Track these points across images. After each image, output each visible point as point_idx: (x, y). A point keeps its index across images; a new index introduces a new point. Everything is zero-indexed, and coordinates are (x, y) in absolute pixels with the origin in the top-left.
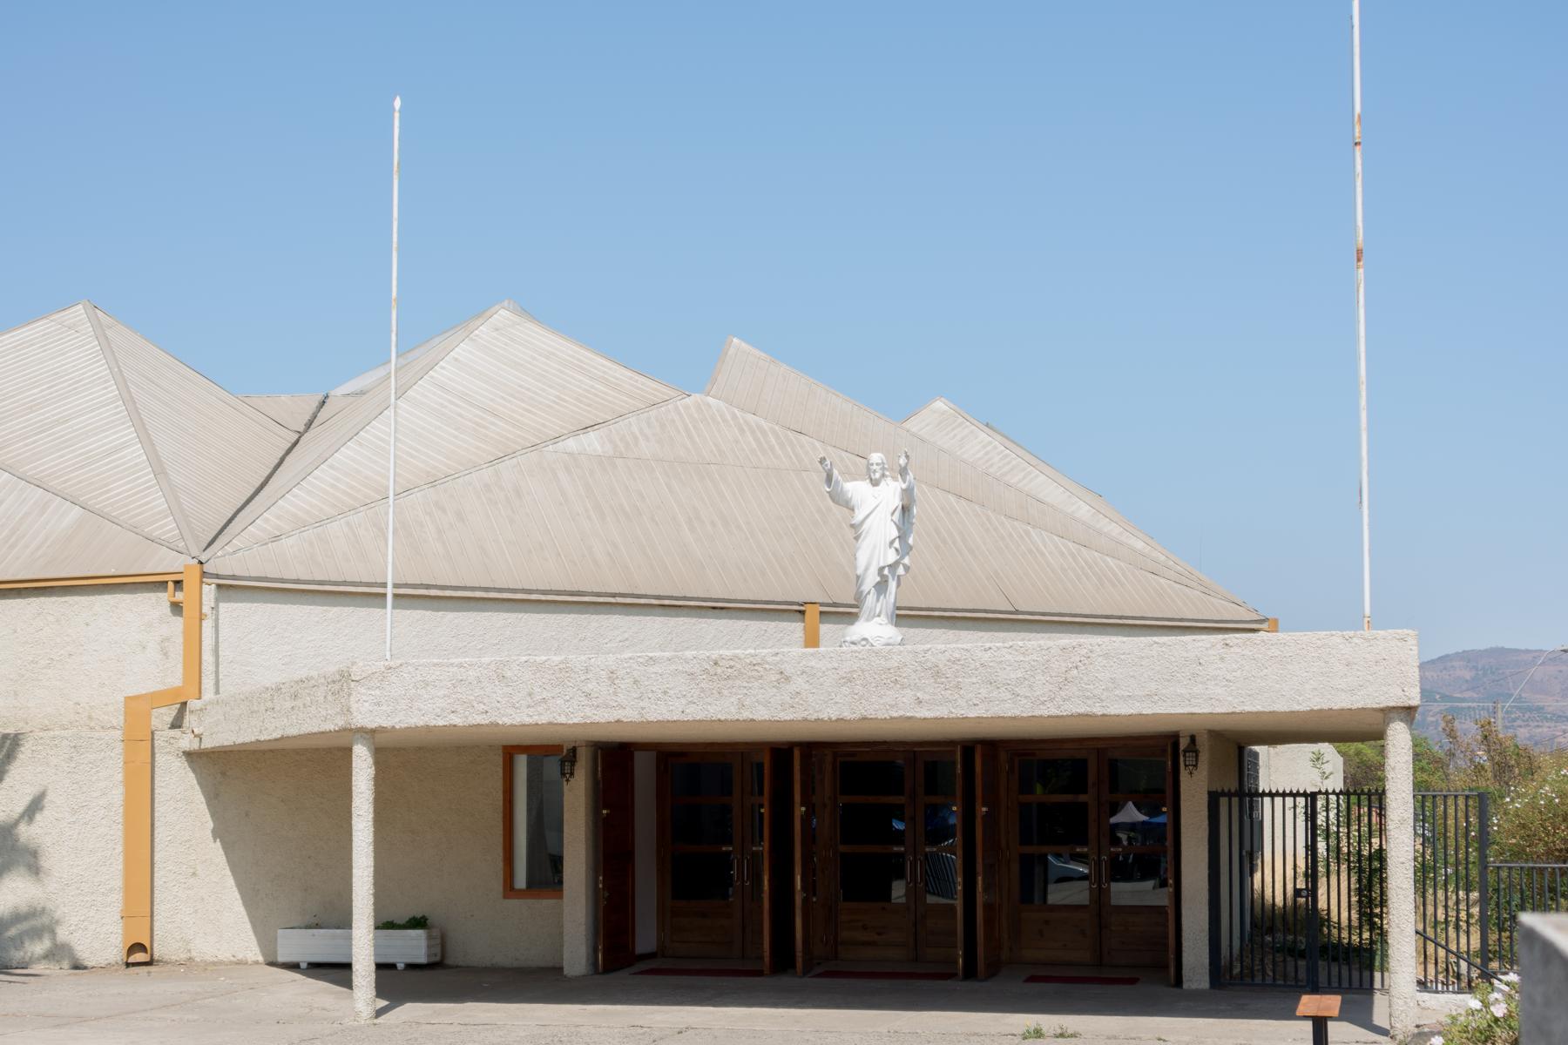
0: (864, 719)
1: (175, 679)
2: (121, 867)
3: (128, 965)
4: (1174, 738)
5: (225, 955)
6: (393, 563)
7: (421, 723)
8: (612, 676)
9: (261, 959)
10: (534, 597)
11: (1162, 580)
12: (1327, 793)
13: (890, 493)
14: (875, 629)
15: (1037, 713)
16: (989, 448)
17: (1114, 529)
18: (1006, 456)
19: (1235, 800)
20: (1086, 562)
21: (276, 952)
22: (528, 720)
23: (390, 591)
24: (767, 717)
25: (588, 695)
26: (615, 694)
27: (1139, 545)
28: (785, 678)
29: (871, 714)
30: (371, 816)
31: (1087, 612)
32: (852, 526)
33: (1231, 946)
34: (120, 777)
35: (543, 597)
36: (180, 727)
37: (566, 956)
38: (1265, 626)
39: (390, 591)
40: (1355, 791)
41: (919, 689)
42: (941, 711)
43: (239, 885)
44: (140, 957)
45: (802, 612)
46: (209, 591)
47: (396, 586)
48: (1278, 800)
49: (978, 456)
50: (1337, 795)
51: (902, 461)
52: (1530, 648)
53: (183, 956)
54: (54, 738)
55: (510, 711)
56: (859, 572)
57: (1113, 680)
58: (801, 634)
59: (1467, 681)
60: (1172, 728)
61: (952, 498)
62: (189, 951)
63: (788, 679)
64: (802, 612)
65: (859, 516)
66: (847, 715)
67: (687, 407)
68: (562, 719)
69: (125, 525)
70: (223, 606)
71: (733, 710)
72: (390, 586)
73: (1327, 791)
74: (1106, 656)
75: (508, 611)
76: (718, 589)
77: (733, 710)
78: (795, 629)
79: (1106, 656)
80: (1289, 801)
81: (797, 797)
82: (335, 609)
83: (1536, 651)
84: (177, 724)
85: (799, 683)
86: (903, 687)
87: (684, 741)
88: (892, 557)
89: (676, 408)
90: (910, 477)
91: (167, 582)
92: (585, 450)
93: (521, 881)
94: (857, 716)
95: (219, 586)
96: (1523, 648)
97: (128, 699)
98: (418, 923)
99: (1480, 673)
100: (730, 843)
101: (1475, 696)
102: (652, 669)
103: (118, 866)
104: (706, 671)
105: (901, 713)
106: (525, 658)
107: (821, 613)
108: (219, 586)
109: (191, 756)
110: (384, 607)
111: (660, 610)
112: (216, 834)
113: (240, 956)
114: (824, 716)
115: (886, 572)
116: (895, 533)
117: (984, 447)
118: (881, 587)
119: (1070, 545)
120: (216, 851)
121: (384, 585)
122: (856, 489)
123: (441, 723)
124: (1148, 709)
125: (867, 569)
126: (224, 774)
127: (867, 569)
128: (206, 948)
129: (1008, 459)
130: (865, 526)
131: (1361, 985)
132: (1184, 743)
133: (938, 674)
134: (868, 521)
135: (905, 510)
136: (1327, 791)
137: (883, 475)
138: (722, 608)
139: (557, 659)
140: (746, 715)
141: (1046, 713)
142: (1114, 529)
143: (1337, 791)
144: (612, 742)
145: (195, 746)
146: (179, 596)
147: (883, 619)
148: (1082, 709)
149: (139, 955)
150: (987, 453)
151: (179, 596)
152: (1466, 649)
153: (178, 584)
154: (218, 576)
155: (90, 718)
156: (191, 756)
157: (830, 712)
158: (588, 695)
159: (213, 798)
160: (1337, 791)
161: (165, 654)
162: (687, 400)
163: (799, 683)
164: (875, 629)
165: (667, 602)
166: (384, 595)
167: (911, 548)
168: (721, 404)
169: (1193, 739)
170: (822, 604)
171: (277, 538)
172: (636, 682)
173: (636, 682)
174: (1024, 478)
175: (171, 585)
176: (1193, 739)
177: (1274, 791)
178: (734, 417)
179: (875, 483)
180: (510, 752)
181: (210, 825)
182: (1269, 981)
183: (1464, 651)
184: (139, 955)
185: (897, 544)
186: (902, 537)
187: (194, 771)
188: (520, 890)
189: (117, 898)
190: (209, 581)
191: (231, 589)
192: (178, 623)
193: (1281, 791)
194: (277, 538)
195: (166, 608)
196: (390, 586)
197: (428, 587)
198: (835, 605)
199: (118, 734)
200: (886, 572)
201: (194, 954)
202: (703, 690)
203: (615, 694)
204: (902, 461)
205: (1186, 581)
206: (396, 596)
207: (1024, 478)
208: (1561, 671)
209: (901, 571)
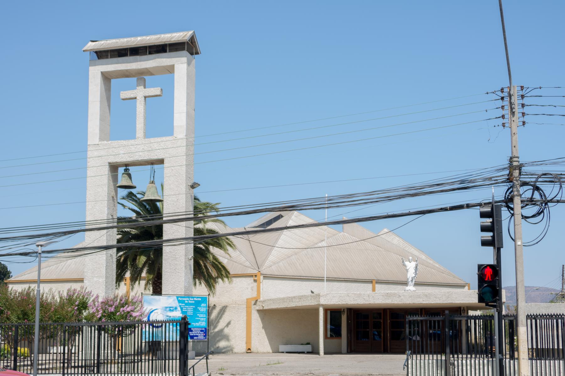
0: (414, 303)
1: (255, 295)
2: (246, 333)
3: (247, 353)
4: (460, 308)
5: (265, 351)
6: (326, 274)
7: (333, 304)
8: (369, 296)
9: (271, 351)
10: (320, 278)
11: (444, 275)
13: (413, 264)
14: (411, 288)
15: (443, 302)
16: (399, 241)
17: (431, 262)
18: (404, 243)
20: (428, 270)
21: (279, 349)
23: (325, 279)
24: (397, 303)
25: (364, 299)
26: (369, 299)
27: (437, 266)
28: (400, 296)
29: (415, 303)
30: (323, 320)
31: (430, 282)
32: (407, 270)
34: (245, 315)
35: (335, 279)
36: (256, 305)
37: (342, 349)
38: (467, 285)
39: (325, 279)
41: (423, 298)
42: (427, 302)
43: (268, 338)
44: (249, 351)
45: (372, 282)
46: (262, 277)
47: (326, 278)
49: (397, 243)
51: (417, 259)
52: (530, 286)
53: (257, 351)
54: (234, 307)
55: (350, 302)
56: (408, 278)
57: (456, 297)
58: (372, 286)
59: (509, 297)
61: (398, 256)
62: (258, 350)
63: (400, 297)
64: (372, 282)
65: (408, 268)
66: (411, 303)
67: (341, 235)
68: (360, 303)
70: (264, 281)
71: (391, 302)
72: (325, 280)
74: (455, 293)
75: (345, 282)
76: (355, 277)
77: (391, 302)
78: (370, 286)
79: (455, 293)
81: (388, 319)
82: (284, 281)
83: (532, 287)
84: (255, 304)
85: (402, 297)
86: (421, 298)
87: (362, 308)
88: (414, 275)
89: (339, 236)
90: (418, 262)
91: (253, 276)
92: (315, 243)
93: (329, 336)
94: (412, 303)
95: (264, 276)
96: (527, 286)
98: (308, 344)
99: (513, 294)
100: (369, 329)
101: (512, 302)
102: (376, 295)
103: (245, 333)
104: (386, 295)
105: (420, 302)
106: (352, 292)
107: (376, 282)
108: (264, 276)
109: (259, 311)
110: (324, 282)
111: (344, 281)
112: (263, 327)
113: (269, 351)
115: (413, 278)
116: (414, 271)
117: (398, 241)
118: (412, 281)
119: (424, 266)
120: (263, 331)
121: (324, 278)
122: (407, 263)
123: (337, 303)
124: (462, 302)
125: (409, 277)
126: (265, 314)
127: (409, 277)
128: (261, 350)
129: (404, 244)
130: (409, 270)
132: (462, 309)
133: (426, 296)
134: (410, 269)
135: (416, 267)
137: (412, 261)
138: (356, 281)
139: (358, 293)
140: (393, 302)
141: (445, 303)
142: (431, 262)
145: (261, 308)
146: (256, 278)
147: (412, 286)
148: (451, 302)
149: (249, 351)
150: (399, 243)
151: (256, 278)
152: (508, 286)
153: (256, 276)
154: (263, 274)
155: (236, 303)
156: (259, 311)
157: (408, 302)
158: (364, 299)
159: (263, 319)
161: (252, 290)
162: (341, 234)
163: (402, 297)
164: (411, 288)
165: (346, 280)
166: (324, 280)
167: (417, 274)
168: (348, 235)
169: (464, 308)
170: (376, 280)
171: (271, 266)
172: (373, 297)
173: (373, 297)
174: (409, 249)
175: (254, 276)
176: (464, 308)
178: (351, 238)
179: (410, 262)
181: (262, 326)
183: (507, 287)
184: (249, 351)
185: (415, 273)
186: (416, 272)
187: (258, 314)
188: (329, 338)
189: (245, 339)
190: (262, 275)
191: (266, 277)
192: (255, 284)
194: (271, 266)
195: (253, 281)
196: (325, 280)
197: (301, 276)
198: (378, 280)
199: (245, 306)
200: (413, 278)
201: (259, 351)
202: (385, 298)
203: (369, 299)
204: (417, 259)
205: (449, 275)
207: (409, 249)
208: (540, 294)
209: (415, 278)
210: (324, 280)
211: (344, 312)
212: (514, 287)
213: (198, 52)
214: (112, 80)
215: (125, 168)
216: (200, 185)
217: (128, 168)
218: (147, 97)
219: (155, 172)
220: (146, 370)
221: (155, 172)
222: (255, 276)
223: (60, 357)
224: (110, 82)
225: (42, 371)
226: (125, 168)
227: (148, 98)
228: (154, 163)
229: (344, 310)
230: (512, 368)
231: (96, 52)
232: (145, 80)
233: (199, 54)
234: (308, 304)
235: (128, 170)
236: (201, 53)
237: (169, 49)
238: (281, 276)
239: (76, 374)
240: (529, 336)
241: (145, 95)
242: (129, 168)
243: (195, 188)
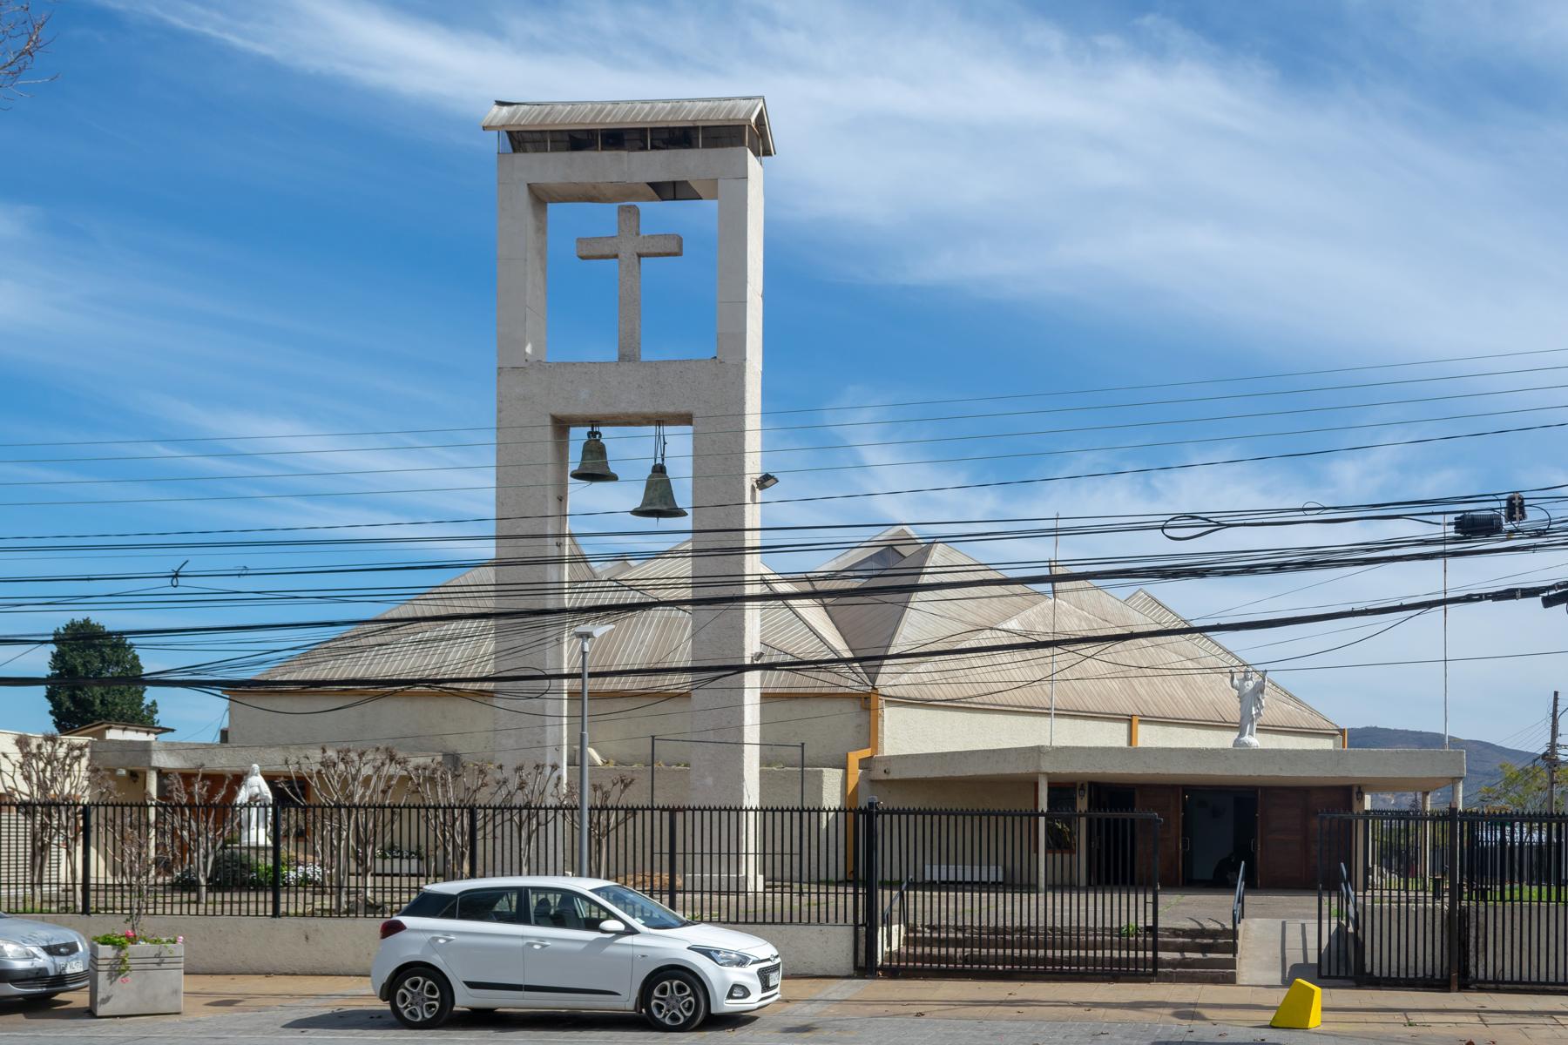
12: (546, 809)
19: (648, 813)
22: (1118, 772)
33: (1062, 877)
39: (566, 696)
40: (460, 806)
47: (1055, 709)
48: (920, 818)
50: (773, 812)
60: (1348, 783)
69: (377, 648)
73: (643, 807)
80: (887, 817)
87: (1121, 782)
97: (860, 760)
114: (1243, 774)
126: (889, 792)
131: (240, 913)
136: (643, 807)
138: (1095, 717)
143: (139, 803)
144: (1116, 784)
160: (139, 803)
177: (124, 803)
180: (1062, 791)
182: (159, 911)
193: (119, 803)
206: (1055, 714)
210: (1050, 714)
211: (1084, 790)
212: (230, 705)
213: (770, 151)
214: (549, 205)
215: (589, 429)
216: (777, 481)
217: (596, 429)
218: (643, 256)
219: (665, 443)
220: (1109, 903)
221: (665, 443)
222: (865, 698)
223: (964, 870)
224: (546, 210)
225: (693, 894)
226: (589, 429)
227: (646, 258)
228: (663, 421)
229: (1082, 785)
230: (1403, 927)
231: (510, 133)
232: (637, 213)
233: (771, 155)
234: (1179, 772)
235: (598, 436)
236: (775, 153)
237: (702, 138)
238: (1024, 707)
239: (236, 902)
240: (553, 848)
241: (638, 252)
242: (602, 429)
243: (766, 487)
